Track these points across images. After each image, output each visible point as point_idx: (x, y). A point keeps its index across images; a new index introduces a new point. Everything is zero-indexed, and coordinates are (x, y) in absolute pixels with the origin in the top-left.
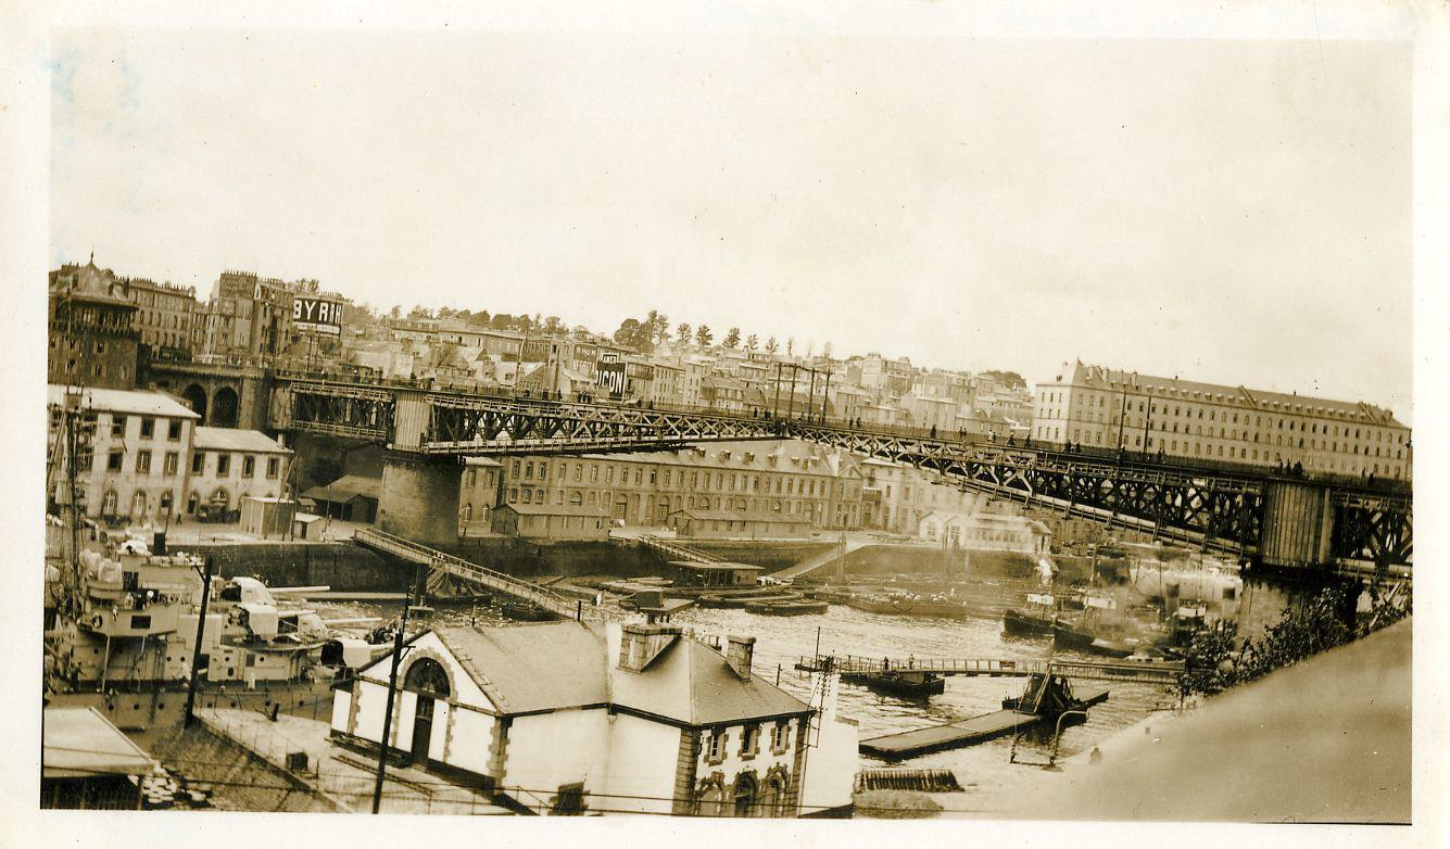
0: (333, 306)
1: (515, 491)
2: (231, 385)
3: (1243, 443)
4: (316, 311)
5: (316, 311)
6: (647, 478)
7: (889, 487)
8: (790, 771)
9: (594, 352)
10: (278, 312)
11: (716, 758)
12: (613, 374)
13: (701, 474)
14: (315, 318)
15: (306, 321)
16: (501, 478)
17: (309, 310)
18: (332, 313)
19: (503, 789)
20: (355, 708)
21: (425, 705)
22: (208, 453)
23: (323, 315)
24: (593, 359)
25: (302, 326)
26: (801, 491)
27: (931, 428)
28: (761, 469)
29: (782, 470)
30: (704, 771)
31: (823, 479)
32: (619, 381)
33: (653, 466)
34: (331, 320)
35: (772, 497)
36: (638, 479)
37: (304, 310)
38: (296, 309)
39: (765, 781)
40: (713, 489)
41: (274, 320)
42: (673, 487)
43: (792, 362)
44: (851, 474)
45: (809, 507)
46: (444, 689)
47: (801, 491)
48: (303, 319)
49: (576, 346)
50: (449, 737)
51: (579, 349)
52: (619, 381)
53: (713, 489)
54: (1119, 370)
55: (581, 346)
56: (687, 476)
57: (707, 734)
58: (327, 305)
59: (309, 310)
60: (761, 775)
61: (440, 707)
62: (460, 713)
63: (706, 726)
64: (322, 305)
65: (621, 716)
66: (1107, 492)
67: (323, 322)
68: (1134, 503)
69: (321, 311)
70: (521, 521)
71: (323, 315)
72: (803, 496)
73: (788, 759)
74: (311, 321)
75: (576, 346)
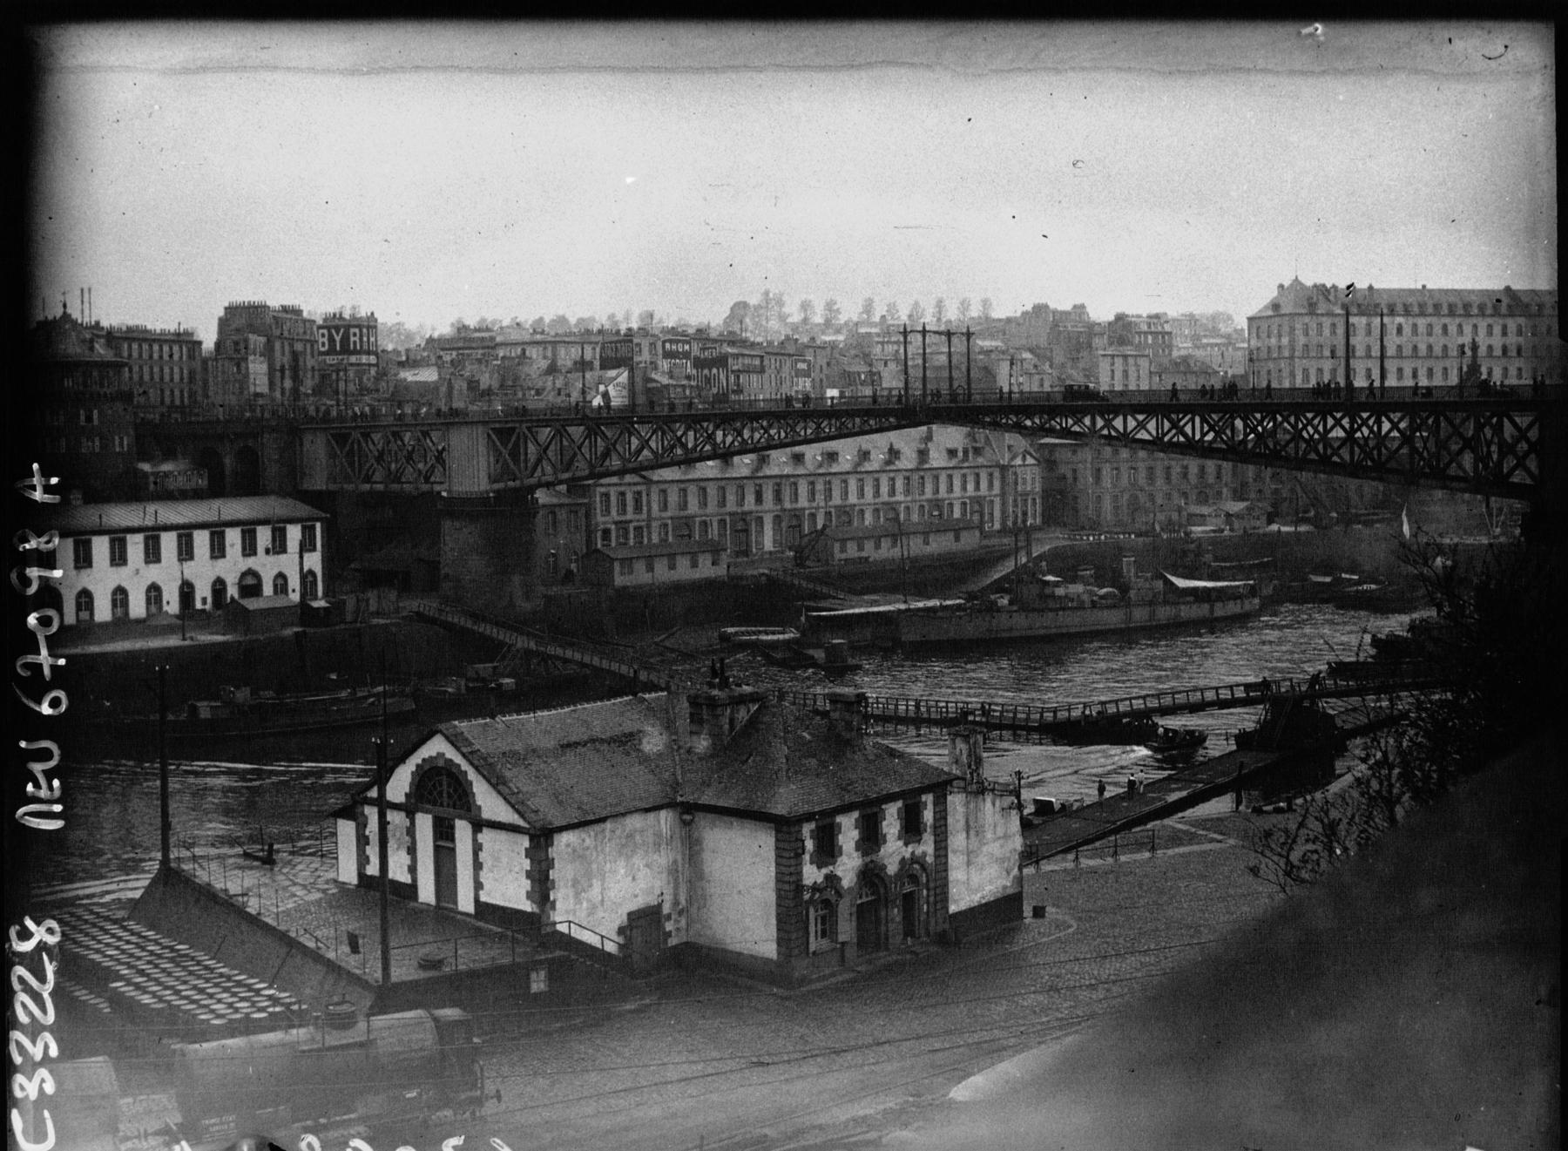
0: (365, 330)
1: (606, 532)
2: (250, 443)
3: (1504, 361)
4: (345, 339)
5: (345, 339)
6: (768, 495)
7: (1075, 471)
8: (930, 859)
9: (687, 347)
10: (299, 347)
11: (827, 851)
12: (714, 371)
13: (692, 489)
14: (346, 350)
15: (337, 353)
16: (588, 515)
17: (338, 339)
18: (365, 339)
19: (555, 923)
20: (362, 842)
21: (444, 833)
22: (129, 537)
23: (355, 342)
24: (686, 355)
25: (330, 360)
26: (964, 488)
27: (1170, 388)
28: (910, 467)
29: (935, 464)
30: (812, 874)
31: (949, 472)
32: (722, 377)
33: (775, 481)
34: (365, 347)
35: (730, 514)
36: (759, 498)
37: (331, 340)
38: (321, 340)
39: (898, 875)
40: (853, 499)
41: (295, 356)
42: (803, 502)
43: (943, 328)
44: (1024, 459)
45: (976, 507)
46: (463, 801)
47: (964, 488)
48: (332, 351)
49: (664, 342)
50: (478, 866)
51: (668, 346)
52: (722, 377)
53: (853, 499)
54: (1342, 285)
55: (671, 341)
56: (820, 487)
57: (807, 829)
58: (357, 331)
59: (338, 339)
60: (892, 868)
61: (462, 829)
62: (486, 836)
63: (809, 817)
64: (352, 330)
65: (699, 816)
66: (1396, 444)
67: (355, 352)
68: (1375, 452)
69: (352, 339)
70: (617, 566)
71: (355, 342)
72: (968, 494)
73: (927, 847)
74: (340, 353)
75: (664, 342)
